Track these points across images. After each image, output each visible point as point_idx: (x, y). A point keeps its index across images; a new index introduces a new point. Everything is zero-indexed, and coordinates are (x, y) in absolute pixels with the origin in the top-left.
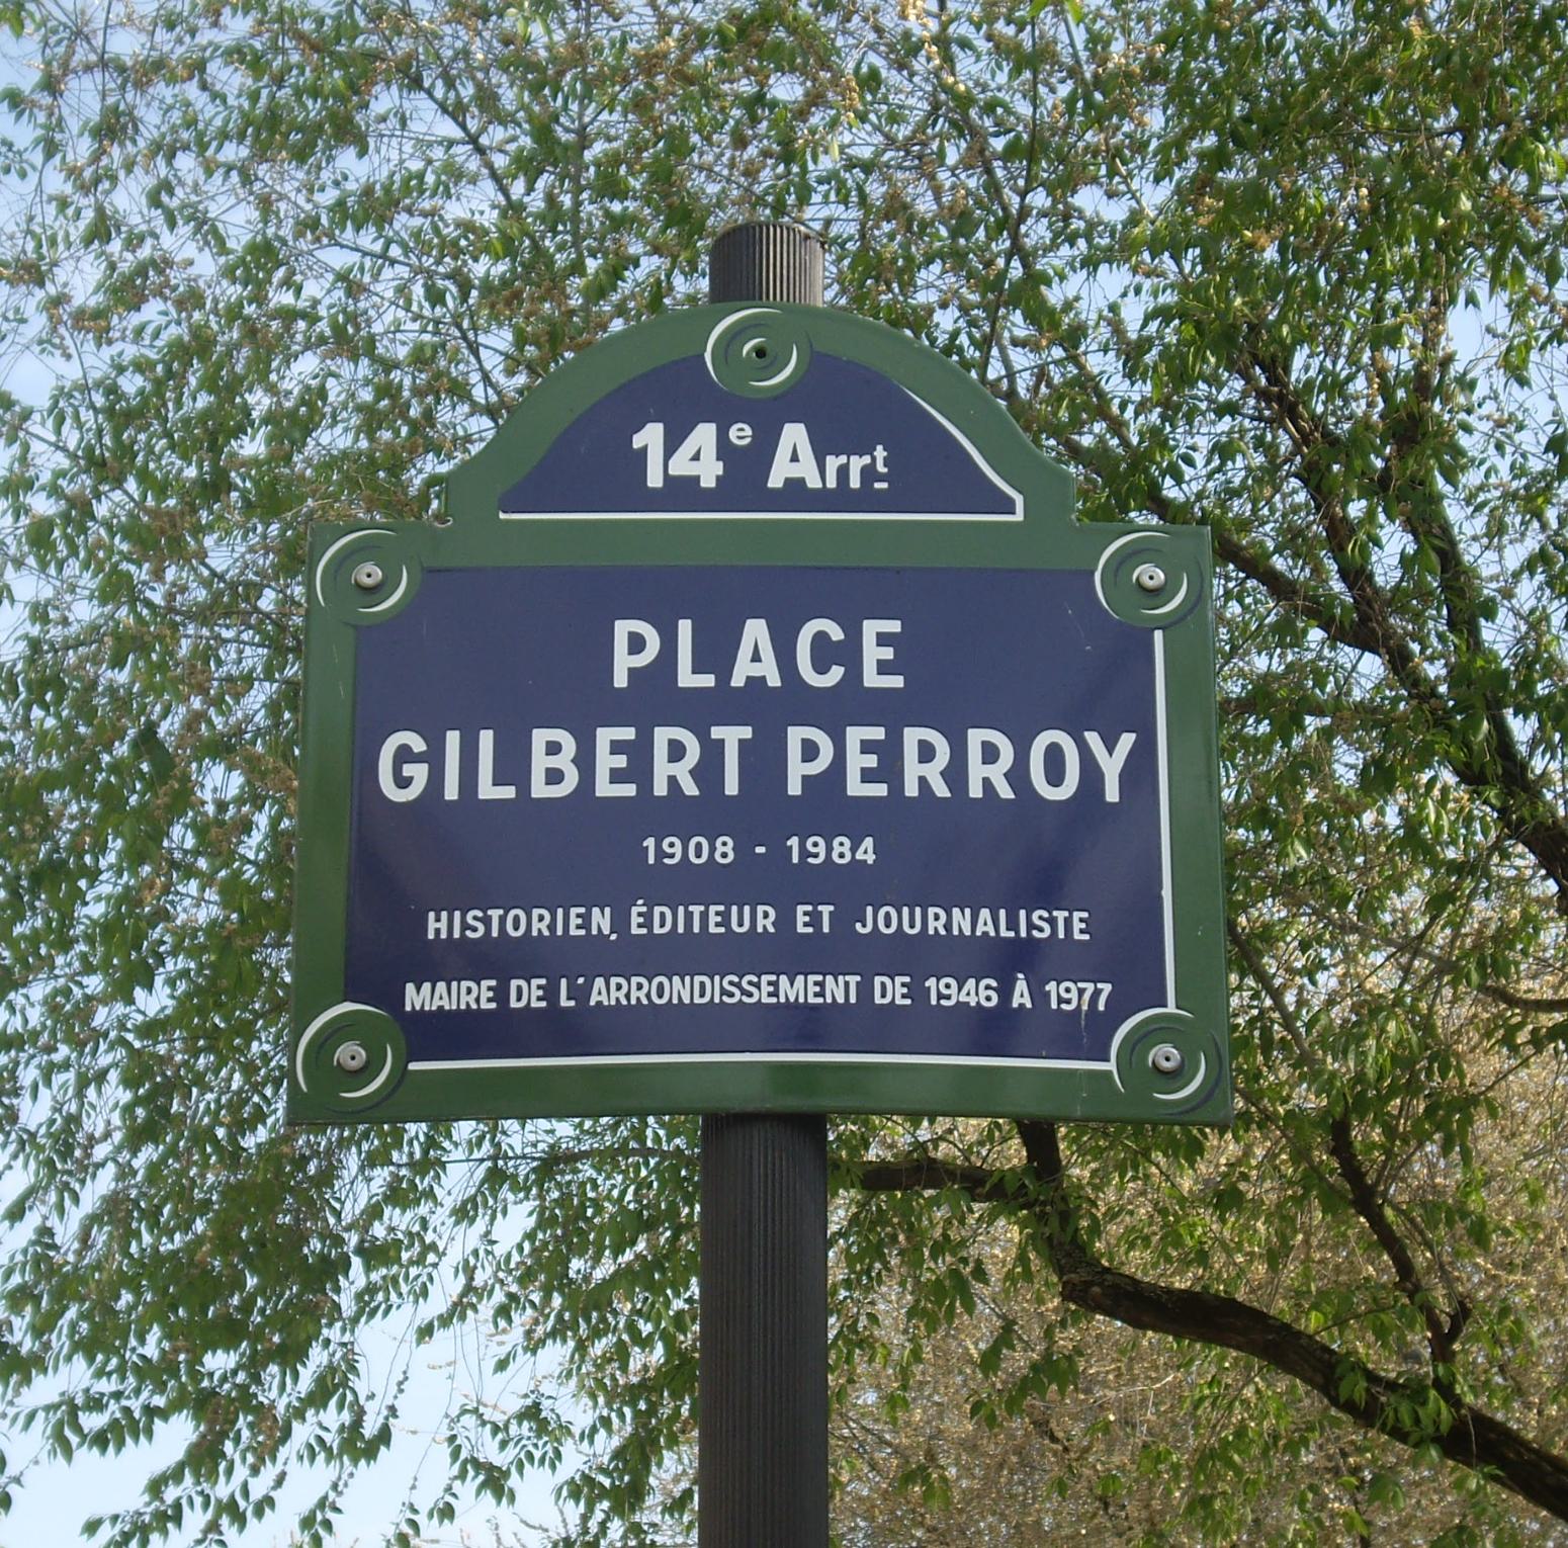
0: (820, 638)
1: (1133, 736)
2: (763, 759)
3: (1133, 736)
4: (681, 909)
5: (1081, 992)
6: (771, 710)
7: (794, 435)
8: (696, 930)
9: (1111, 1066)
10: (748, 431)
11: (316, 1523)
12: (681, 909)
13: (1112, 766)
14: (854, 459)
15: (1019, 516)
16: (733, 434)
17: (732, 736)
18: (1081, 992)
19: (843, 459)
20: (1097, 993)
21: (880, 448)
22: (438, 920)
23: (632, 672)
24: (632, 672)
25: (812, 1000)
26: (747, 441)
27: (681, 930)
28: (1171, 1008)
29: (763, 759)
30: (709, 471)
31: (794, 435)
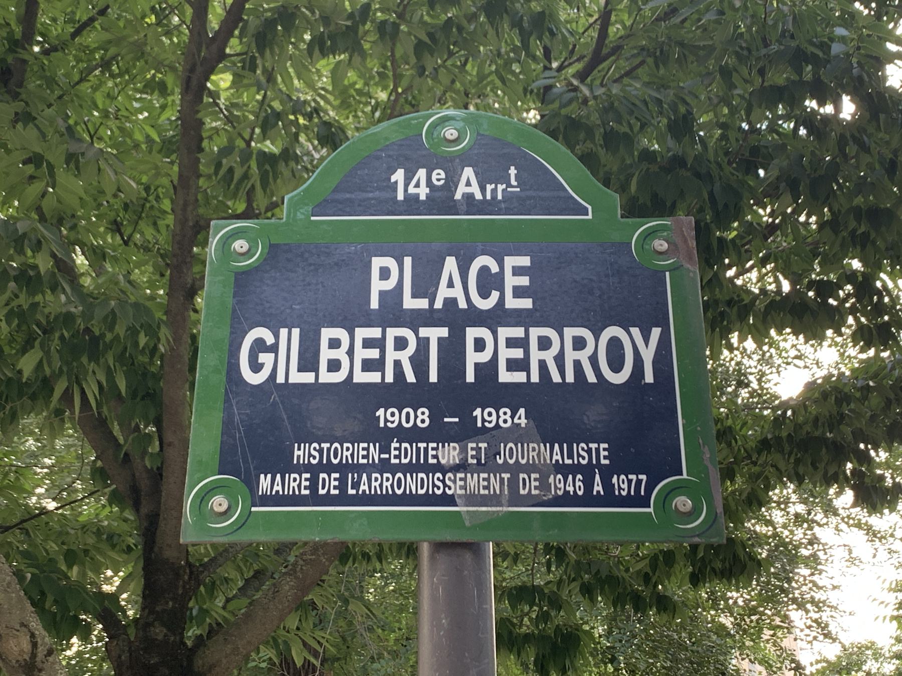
0: (484, 270)
1: (659, 329)
2: (452, 351)
3: (659, 329)
4: (414, 444)
5: (630, 481)
6: (456, 318)
7: (468, 172)
8: (422, 461)
9: (651, 510)
10: (443, 175)
11: (1, 101)
12: (414, 444)
13: (648, 355)
14: (499, 186)
15: (590, 217)
16: (434, 177)
17: (435, 334)
18: (630, 481)
19: (493, 186)
20: (639, 482)
21: (512, 168)
22: (299, 449)
23: (382, 294)
24: (382, 294)
25: (482, 492)
26: (442, 182)
27: (414, 461)
28: (685, 476)
29: (452, 351)
30: (423, 192)
31: (468, 172)
